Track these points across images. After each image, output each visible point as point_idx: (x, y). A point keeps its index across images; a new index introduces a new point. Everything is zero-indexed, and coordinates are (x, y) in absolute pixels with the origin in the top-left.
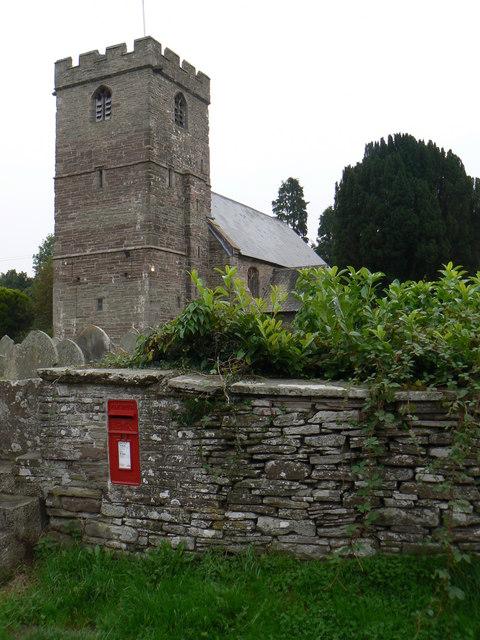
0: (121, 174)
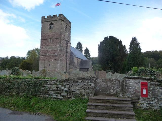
0: (55, 40)
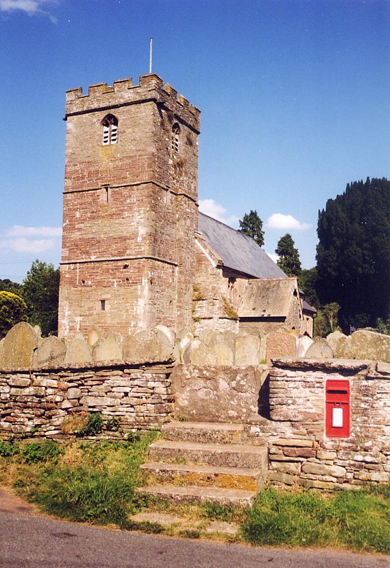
0: (125, 192)
